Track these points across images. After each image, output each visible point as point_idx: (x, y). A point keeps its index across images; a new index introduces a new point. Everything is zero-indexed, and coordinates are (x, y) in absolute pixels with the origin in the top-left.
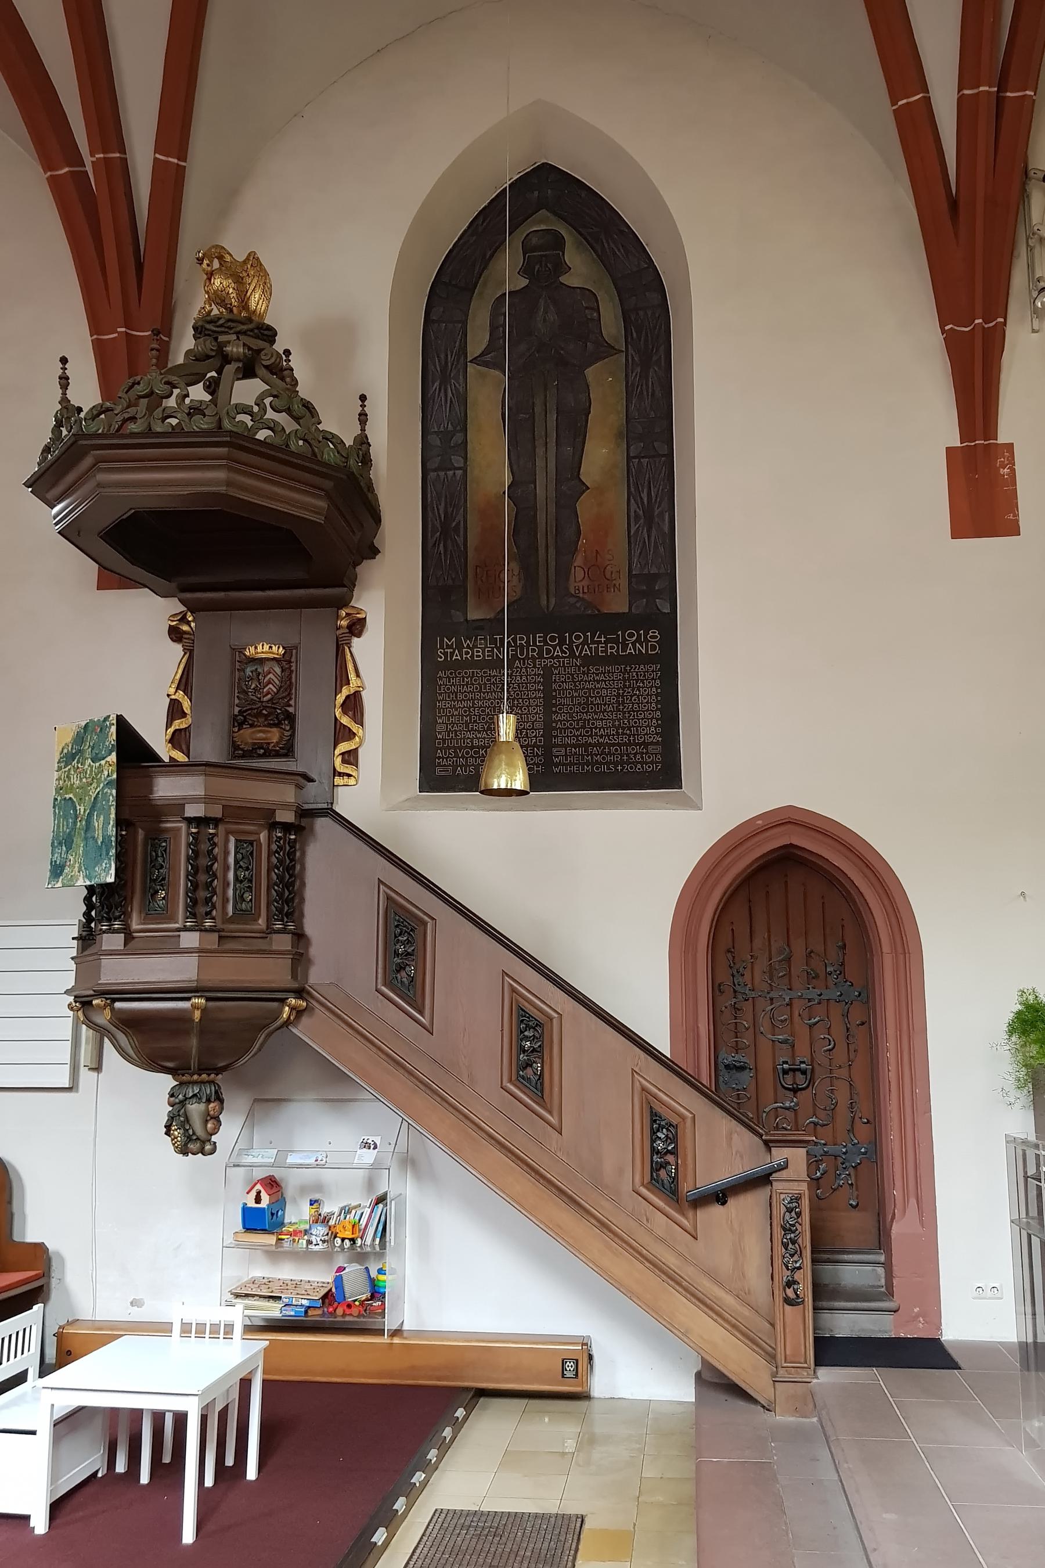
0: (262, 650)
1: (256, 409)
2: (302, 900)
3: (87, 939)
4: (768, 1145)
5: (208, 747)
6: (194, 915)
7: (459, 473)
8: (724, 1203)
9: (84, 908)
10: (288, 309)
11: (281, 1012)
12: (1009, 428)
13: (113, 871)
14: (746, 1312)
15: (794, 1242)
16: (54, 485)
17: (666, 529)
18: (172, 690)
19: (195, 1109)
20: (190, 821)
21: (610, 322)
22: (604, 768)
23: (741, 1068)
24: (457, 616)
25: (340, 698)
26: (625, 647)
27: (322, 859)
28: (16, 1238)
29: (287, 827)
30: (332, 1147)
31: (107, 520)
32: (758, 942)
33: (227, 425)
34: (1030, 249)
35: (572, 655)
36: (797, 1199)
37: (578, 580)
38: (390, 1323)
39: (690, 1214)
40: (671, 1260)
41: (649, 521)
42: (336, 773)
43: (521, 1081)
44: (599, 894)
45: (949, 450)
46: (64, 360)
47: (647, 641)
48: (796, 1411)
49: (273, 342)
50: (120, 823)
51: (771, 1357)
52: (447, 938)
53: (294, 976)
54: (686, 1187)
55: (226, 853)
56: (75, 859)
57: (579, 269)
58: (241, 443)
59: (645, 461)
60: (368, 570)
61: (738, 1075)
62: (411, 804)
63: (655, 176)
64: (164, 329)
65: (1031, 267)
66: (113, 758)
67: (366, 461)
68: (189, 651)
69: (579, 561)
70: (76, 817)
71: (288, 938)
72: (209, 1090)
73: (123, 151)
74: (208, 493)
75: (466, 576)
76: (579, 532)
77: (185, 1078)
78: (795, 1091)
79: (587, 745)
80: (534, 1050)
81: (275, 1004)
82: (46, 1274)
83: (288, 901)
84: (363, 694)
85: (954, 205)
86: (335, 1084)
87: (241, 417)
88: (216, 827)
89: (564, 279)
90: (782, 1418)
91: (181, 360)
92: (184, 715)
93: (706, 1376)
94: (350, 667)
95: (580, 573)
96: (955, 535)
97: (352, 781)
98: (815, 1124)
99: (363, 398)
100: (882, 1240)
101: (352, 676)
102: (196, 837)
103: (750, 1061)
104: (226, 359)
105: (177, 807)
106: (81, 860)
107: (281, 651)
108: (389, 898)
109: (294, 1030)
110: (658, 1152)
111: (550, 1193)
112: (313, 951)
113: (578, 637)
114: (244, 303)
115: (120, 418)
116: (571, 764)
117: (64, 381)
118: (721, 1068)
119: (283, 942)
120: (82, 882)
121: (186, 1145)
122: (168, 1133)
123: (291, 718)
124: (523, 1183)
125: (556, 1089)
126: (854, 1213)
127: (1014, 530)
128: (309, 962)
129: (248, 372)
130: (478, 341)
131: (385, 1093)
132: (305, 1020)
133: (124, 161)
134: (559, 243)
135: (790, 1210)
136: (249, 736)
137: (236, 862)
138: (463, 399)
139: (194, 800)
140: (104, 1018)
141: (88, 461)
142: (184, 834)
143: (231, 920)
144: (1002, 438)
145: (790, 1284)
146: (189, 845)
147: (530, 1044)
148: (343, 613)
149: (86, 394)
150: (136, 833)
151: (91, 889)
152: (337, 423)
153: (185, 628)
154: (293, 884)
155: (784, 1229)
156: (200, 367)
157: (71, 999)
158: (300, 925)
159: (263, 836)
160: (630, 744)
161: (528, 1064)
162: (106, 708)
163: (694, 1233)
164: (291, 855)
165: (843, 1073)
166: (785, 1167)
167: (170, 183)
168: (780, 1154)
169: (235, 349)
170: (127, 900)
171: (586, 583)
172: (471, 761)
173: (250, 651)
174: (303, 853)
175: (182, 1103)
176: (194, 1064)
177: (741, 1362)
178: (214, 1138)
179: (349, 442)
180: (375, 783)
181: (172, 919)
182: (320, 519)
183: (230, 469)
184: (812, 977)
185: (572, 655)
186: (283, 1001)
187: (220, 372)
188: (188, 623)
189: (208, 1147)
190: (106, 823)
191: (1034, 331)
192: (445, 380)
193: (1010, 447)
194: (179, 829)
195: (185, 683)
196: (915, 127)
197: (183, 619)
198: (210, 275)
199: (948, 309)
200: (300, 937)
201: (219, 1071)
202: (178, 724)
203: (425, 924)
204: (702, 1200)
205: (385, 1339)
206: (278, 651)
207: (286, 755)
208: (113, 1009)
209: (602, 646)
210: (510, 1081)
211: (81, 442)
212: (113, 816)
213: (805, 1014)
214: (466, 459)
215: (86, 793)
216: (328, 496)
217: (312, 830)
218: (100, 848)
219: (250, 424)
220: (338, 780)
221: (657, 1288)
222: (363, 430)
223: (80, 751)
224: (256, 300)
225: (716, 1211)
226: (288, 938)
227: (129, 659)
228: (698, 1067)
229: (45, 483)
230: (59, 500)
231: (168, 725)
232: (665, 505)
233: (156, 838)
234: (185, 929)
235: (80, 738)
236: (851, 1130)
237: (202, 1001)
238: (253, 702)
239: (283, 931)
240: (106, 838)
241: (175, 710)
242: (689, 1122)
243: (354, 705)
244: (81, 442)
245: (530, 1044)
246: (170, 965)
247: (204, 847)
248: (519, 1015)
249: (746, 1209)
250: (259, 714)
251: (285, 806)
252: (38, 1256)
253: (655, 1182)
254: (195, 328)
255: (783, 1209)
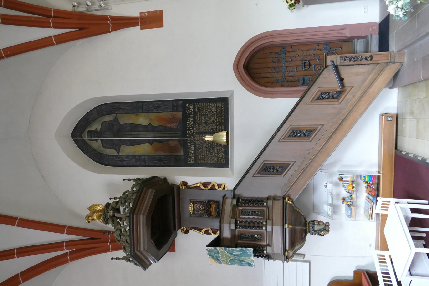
0: (191, 209)
1: (124, 207)
2: (258, 198)
3: (268, 257)
4: (327, 66)
5: (216, 224)
6: (262, 227)
7: (146, 157)
8: (343, 79)
9: (260, 258)
10: (102, 200)
11: (289, 203)
12: (136, 14)
13: (250, 249)
14: (374, 71)
15: (354, 58)
16: (145, 262)
17: (160, 103)
18: (201, 233)
19: (316, 228)
20: (236, 228)
21: (109, 118)
22: (223, 118)
23: (304, 79)
24: (183, 157)
25: (204, 188)
26: (191, 113)
27: (246, 192)
28: (352, 279)
29: (238, 202)
30: (325, 191)
31: (154, 249)
32: (270, 76)
33: (128, 215)
34: (92, 11)
35: (193, 127)
36: (342, 58)
37: (173, 126)
38: (376, 174)
39: (346, 88)
40: (360, 93)
41: (159, 107)
42: (224, 190)
43: (309, 136)
44: (255, 118)
45: (141, 29)
46: (112, 259)
47: (189, 107)
48: (404, 55)
49: (110, 204)
50: (236, 246)
51: (387, 63)
52: (267, 158)
53: (279, 200)
54: (339, 90)
55: (245, 218)
56: (246, 260)
57: (96, 126)
58: (133, 211)
59: (143, 109)
60: (170, 181)
61: (306, 81)
62: (232, 170)
63: (73, 106)
64: (105, 232)
65: (96, 10)
66: (218, 248)
67: (139, 179)
68: (191, 228)
69: (168, 125)
70: (234, 259)
71: (269, 201)
72: (311, 224)
73: (63, 242)
74: (146, 220)
75: (172, 155)
76: (161, 126)
77: (308, 230)
78: (310, 65)
79: (217, 123)
80: (300, 132)
81: (287, 205)
82: (363, 271)
83: (259, 201)
84: (203, 182)
85: (80, 29)
86: (309, 190)
87: (126, 211)
88: (238, 221)
89: (99, 130)
90: (406, 59)
91: (114, 228)
92: (208, 230)
93: (391, 85)
94: (195, 185)
95: (172, 125)
96: (162, 26)
97: (226, 185)
98: (319, 60)
99: (124, 180)
100: (351, 40)
101: (198, 185)
102: (240, 226)
103: (302, 77)
104: (114, 216)
105: (232, 231)
106: (246, 258)
107: (191, 204)
108: (258, 174)
109: (295, 200)
110: (329, 97)
111: (340, 128)
112: (272, 194)
113: (188, 125)
114: (100, 211)
115: (126, 244)
116: (222, 127)
117: (117, 259)
118: (304, 83)
119: (270, 203)
120: (252, 258)
121: (327, 230)
122: (323, 236)
123: (209, 201)
124: (338, 135)
125: (311, 126)
126: (343, 48)
127: (161, 11)
128: (275, 196)
129: (118, 210)
130: (113, 152)
131: (312, 175)
132: (291, 197)
133: (67, 242)
134: (90, 132)
135: (345, 60)
136: (214, 212)
137: (247, 215)
138: (128, 156)
139: (230, 226)
140: (291, 253)
141: (138, 253)
142: (240, 230)
143: (264, 217)
144: (138, 15)
145: (366, 59)
146: (242, 228)
147: (298, 134)
148: (181, 187)
149: (121, 254)
150: (239, 243)
151: (255, 256)
152: (128, 186)
153: (185, 229)
154: (254, 200)
155: (350, 61)
156: (115, 223)
157: (285, 262)
158: (265, 198)
159: (240, 208)
160: (216, 111)
161: (304, 134)
162: (204, 250)
163: (351, 88)
164: (246, 201)
165: (305, 52)
166: (333, 62)
167: (72, 230)
168: (329, 63)
169: (111, 213)
170: (258, 246)
171: (174, 124)
172: (221, 154)
173: (191, 212)
174: (245, 197)
175: (315, 231)
176: (304, 228)
177: (388, 74)
178: (325, 223)
179: (134, 183)
180: (226, 179)
181: (263, 233)
182: (154, 191)
183: (140, 214)
184: (279, 61)
185: (193, 127)
186: (286, 203)
187: (118, 218)
188: (184, 228)
189: (327, 224)
190: (236, 251)
191: (112, 9)
192: (124, 161)
193: (141, 13)
194: (238, 231)
195: (200, 230)
196: (61, 40)
197: (183, 230)
198: (93, 220)
199: (105, 31)
200: (268, 198)
201: (306, 221)
202: (210, 232)
203: (265, 164)
204: (343, 85)
205: (381, 175)
206: (191, 205)
207: (219, 203)
208: (288, 250)
209: (190, 119)
210: (309, 139)
211: (132, 254)
212: (234, 249)
213: (289, 63)
214: (142, 155)
215: (228, 256)
216: (148, 189)
217: (239, 195)
218: (243, 252)
219: (128, 209)
220: (226, 189)
221: (367, 97)
222: (132, 180)
223: (216, 257)
224: (100, 208)
225: (345, 81)
226: (269, 201)
227: (192, 244)
228: (303, 90)
229: (145, 265)
230: (149, 261)
231: (211, 234)
232: (154, 103)
233: (240, 237)
234: (266, 229)
235: (213, 257)
236: (321, 50)
237: (286, 225)
238: (205, 212)
239: (267, 203)
240: (240, 251)
241: (207, 232)
242: (320, 89)
243: (205, 185)
244: (132, 254)
245: (298, 134)
246: (276, 234)
247: (243, 224)
248: (291, 137)
249: (345, 72)
250: (208, 210)
251: (232, 202)
252: (357, 273)
253: (338, 98)
254: (106, 224)
255: (345, 61)
